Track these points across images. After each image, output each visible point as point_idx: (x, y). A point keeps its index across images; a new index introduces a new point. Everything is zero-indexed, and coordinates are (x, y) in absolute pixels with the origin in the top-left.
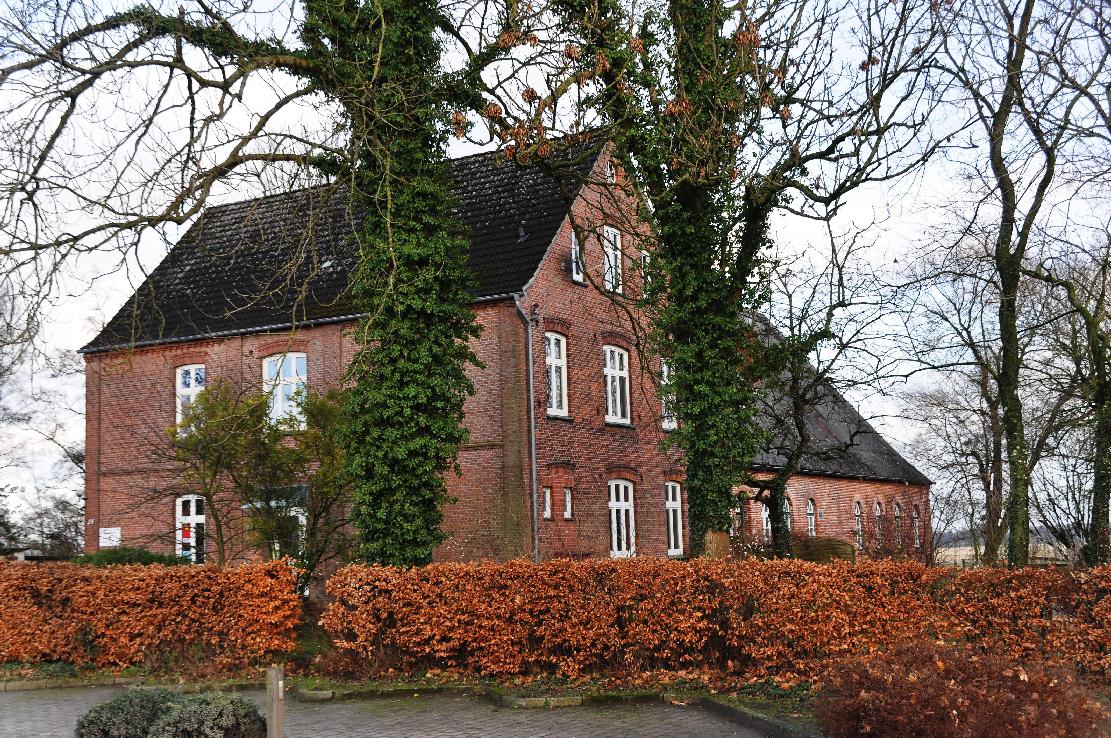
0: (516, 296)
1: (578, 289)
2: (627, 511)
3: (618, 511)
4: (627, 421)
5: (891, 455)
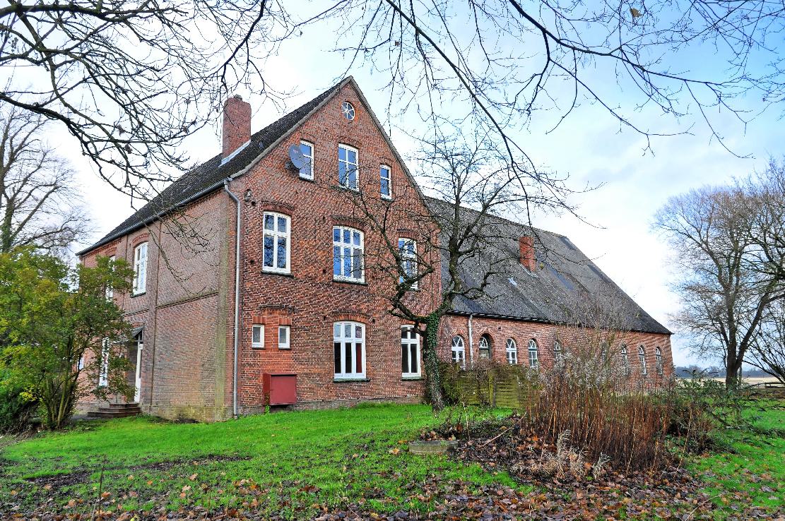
0: (225, 182)
2: (358, 346)
3: (348, 346)
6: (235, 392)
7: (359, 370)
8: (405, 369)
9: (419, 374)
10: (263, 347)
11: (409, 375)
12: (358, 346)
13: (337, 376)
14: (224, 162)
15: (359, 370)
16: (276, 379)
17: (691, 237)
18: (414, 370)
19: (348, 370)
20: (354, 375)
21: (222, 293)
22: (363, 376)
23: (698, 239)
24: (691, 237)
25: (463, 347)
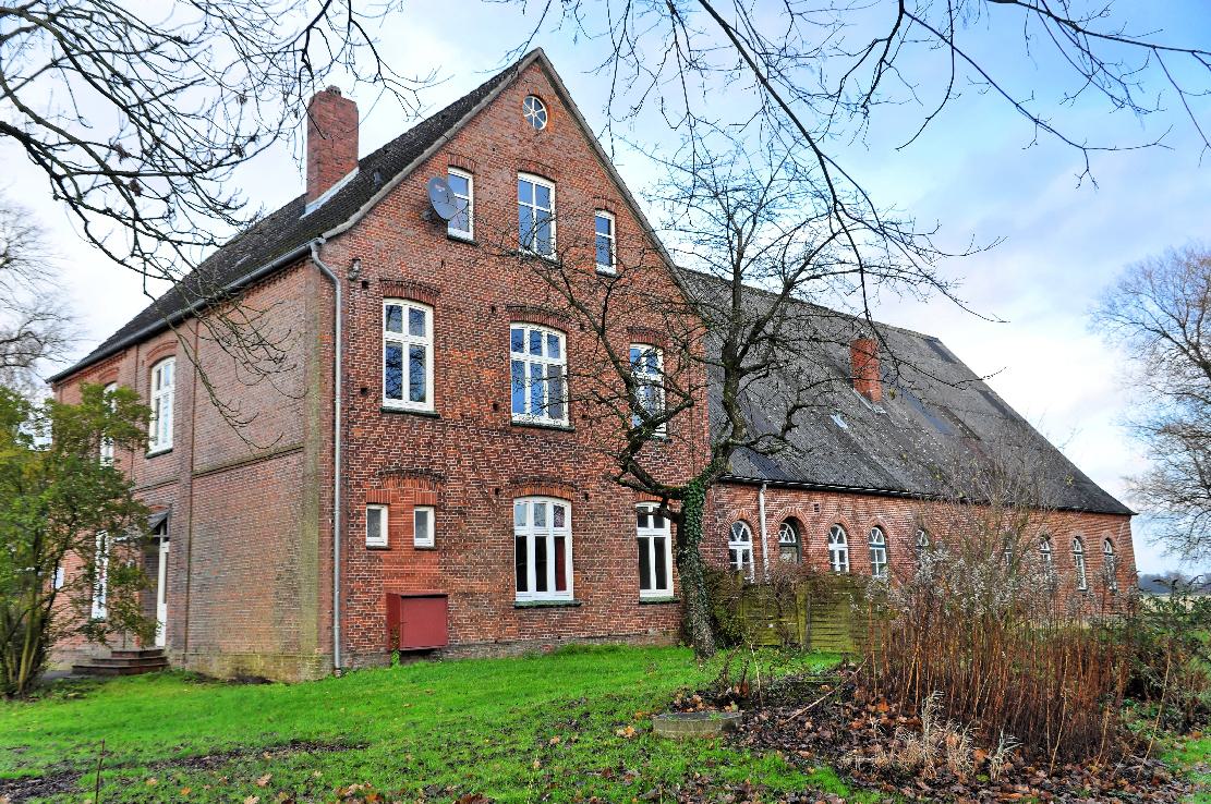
1: (457, 253)
2: (559, 541)
3: (541, 542)
4: (565, 423)
5: (1081, 482)
6: (336, 626)
7: (560, 585)
8: (645, 584)
9: (668, 593)
10: (432, 545)
11: (652, 593)
12: (559, 541)
13: (522, 598)
14: (310, 209)
15: (560, 585)
16: (408, 603)
17: (1168, 337)
18: (661, 585)
19: (542, 586)
20: (551, 595)
21: (310, 451)
22: (568, 596)
23: (1180, 338)
24: (1168, 337)
25: (845, 545)
